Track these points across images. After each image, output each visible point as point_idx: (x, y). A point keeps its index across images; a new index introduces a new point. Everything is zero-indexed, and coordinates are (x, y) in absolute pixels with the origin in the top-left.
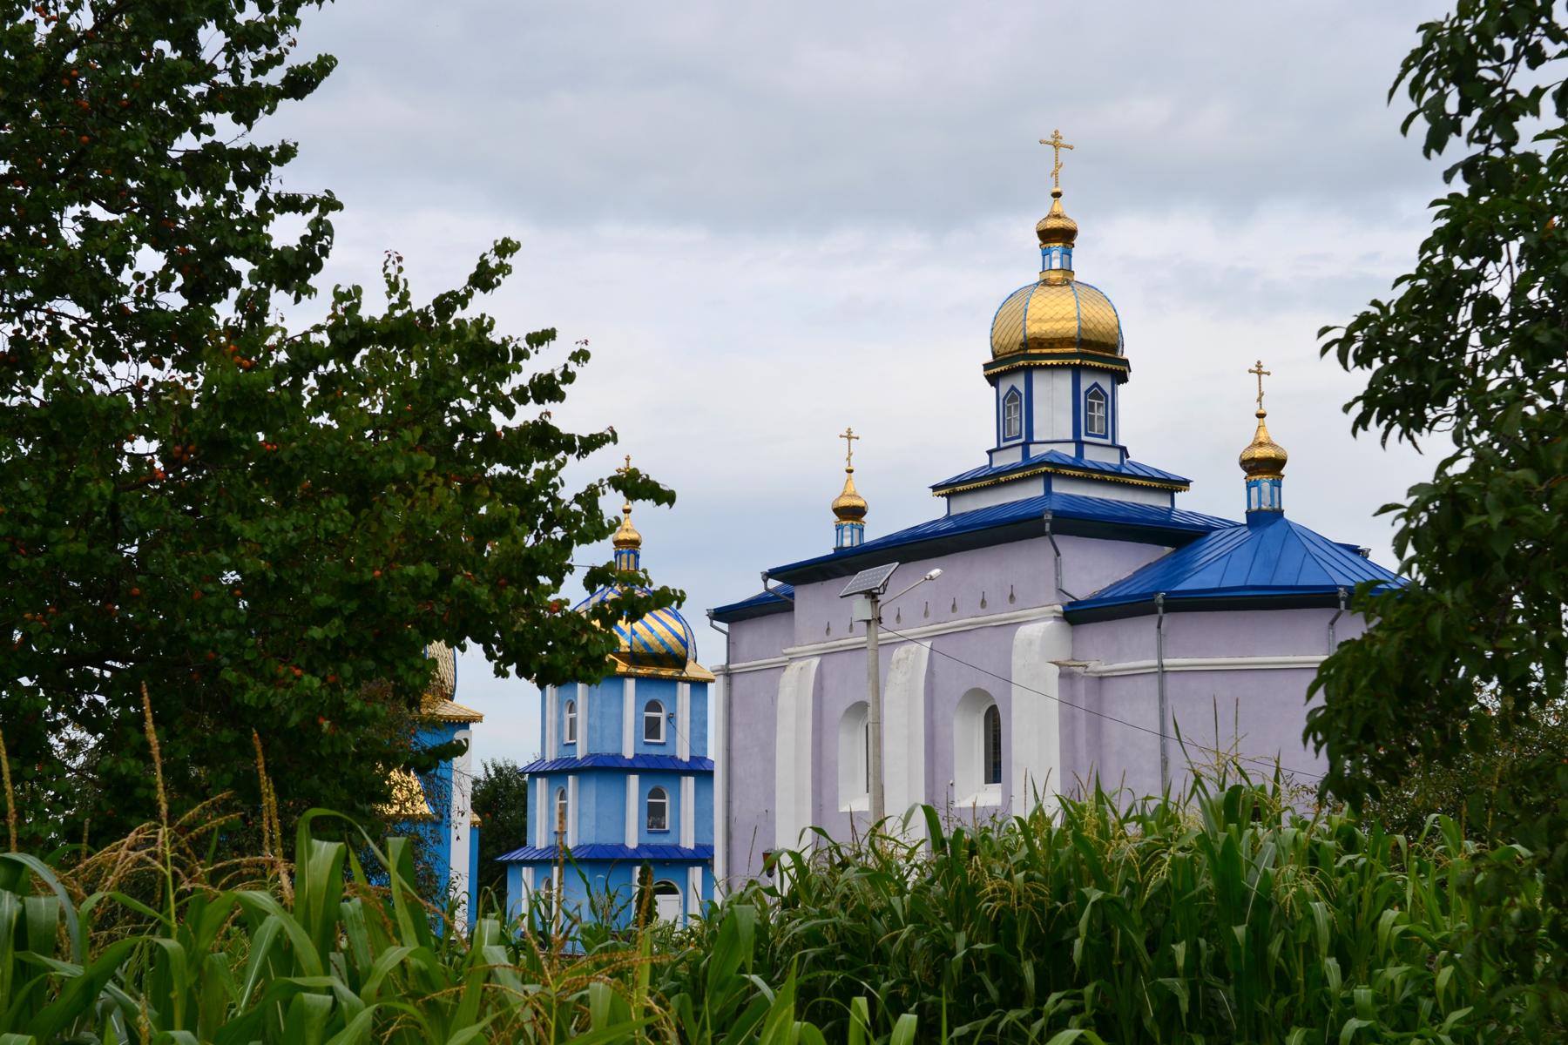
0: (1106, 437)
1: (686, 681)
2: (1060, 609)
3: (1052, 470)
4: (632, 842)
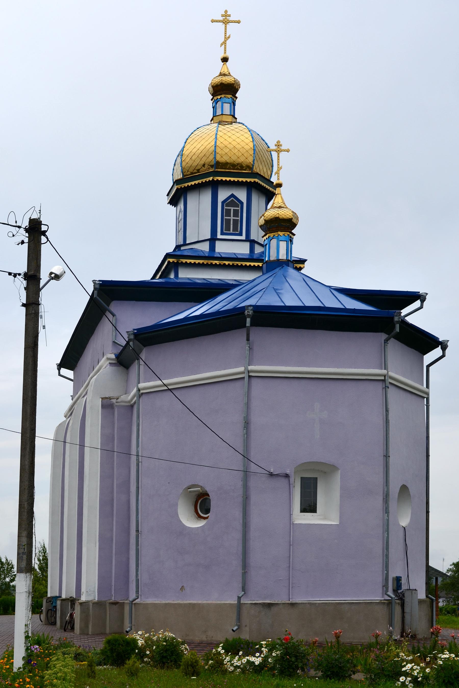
2: (113, 356)
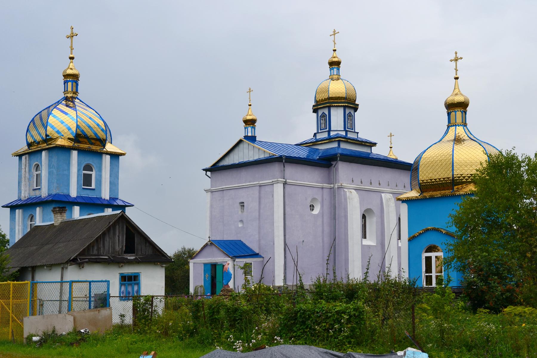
0: (352, 129)
1: (107, 153)
3: (339, 139)
4: (74, 193)
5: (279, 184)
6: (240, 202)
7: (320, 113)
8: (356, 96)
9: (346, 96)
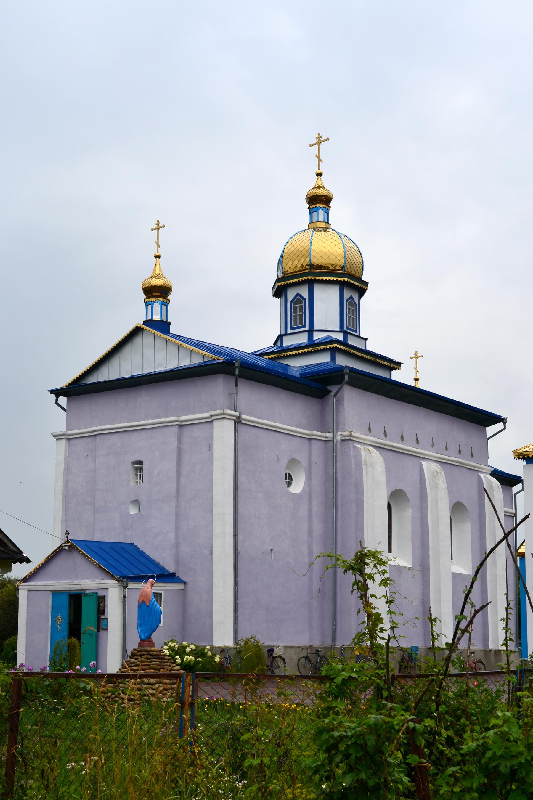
5: (225, 422)
6: (134, 460)
7: (291, 294)
8: (363, 266)
9: (345, 263)
